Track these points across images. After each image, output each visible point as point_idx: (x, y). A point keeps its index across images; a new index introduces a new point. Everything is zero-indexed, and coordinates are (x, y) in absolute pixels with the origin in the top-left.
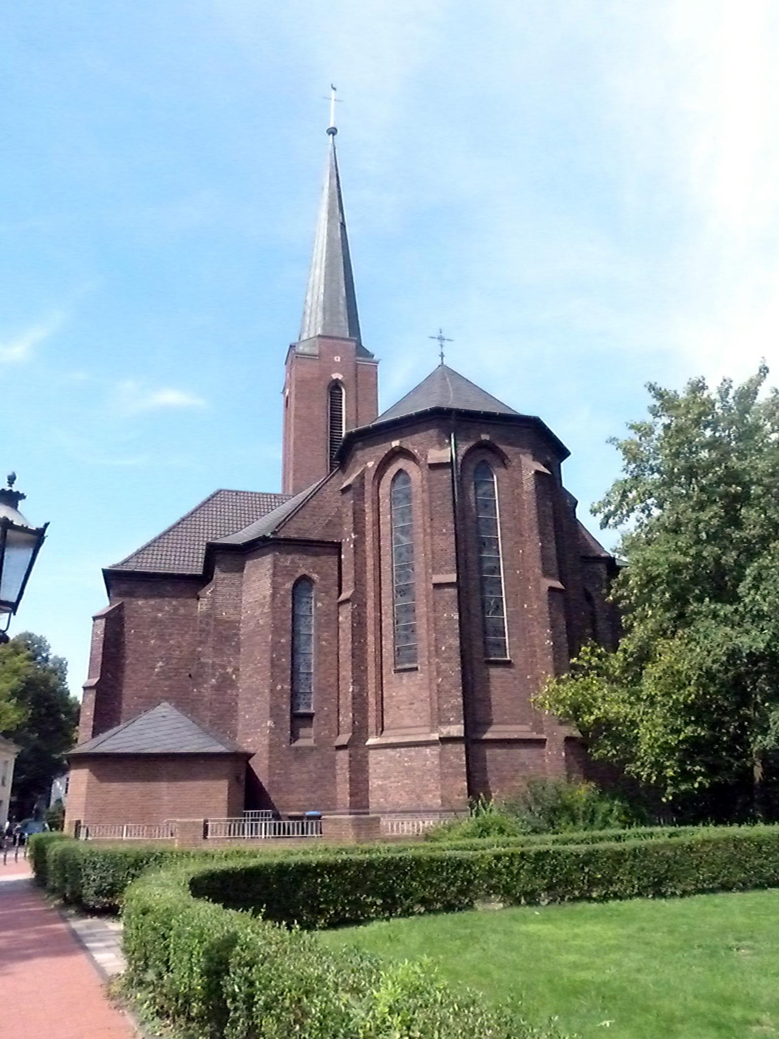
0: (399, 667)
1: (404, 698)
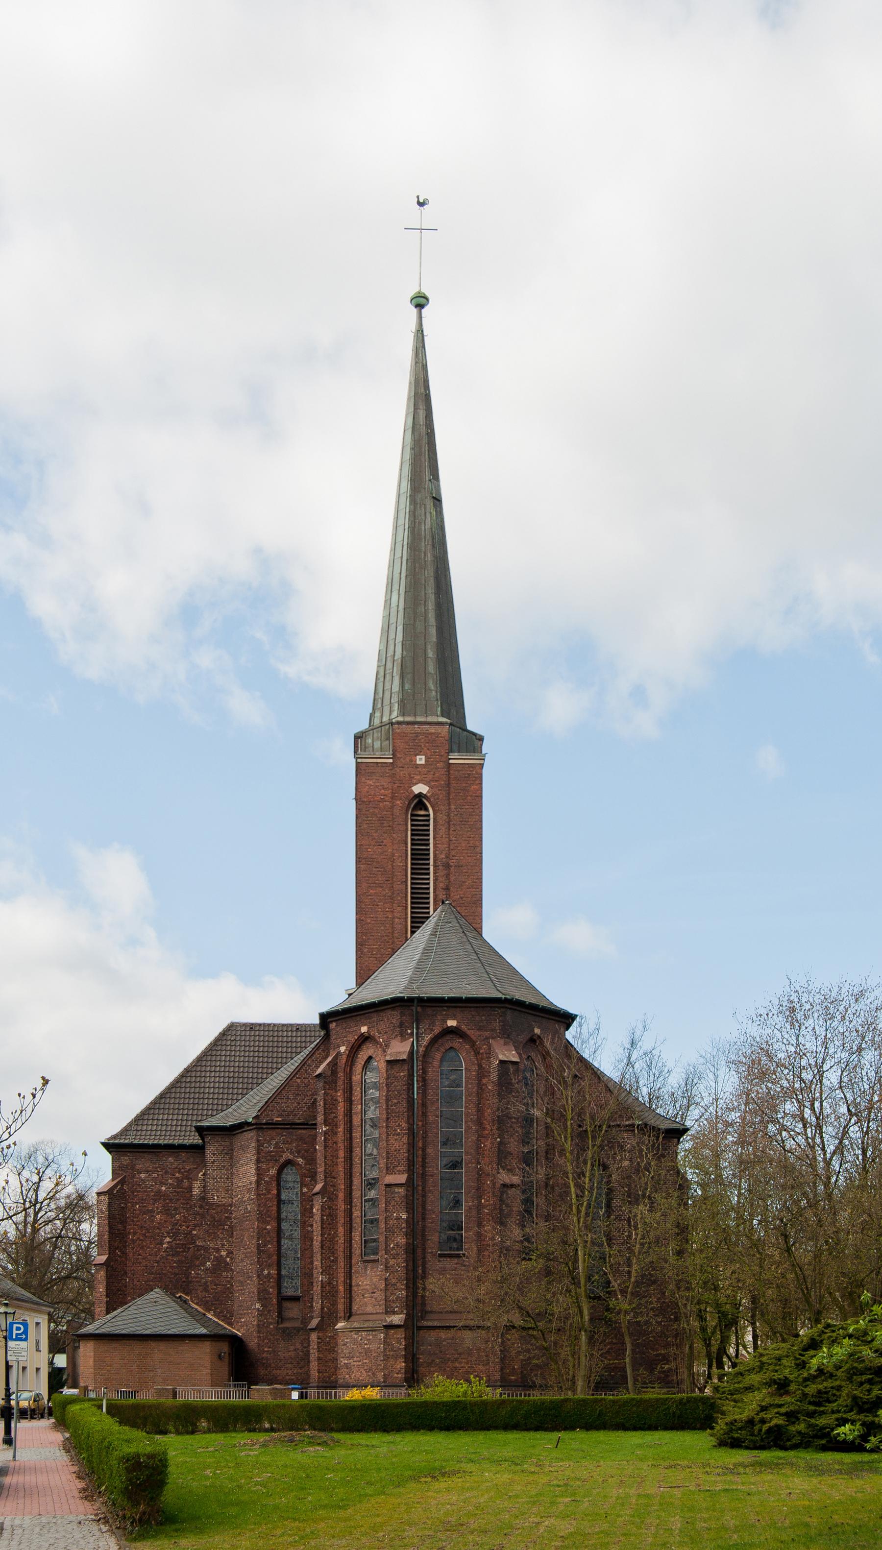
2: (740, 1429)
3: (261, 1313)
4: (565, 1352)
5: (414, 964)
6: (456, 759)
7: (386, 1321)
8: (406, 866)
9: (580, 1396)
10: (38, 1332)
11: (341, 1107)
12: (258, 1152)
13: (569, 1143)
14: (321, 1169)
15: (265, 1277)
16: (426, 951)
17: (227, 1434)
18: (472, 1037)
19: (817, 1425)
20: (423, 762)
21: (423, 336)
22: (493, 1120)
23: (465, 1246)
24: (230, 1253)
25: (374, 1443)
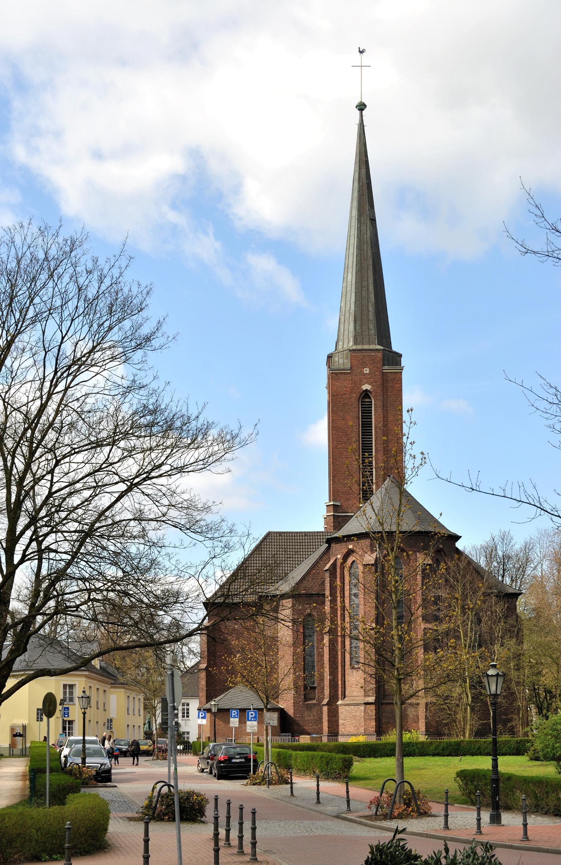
6: (387, 369)
9: (467, 739)
20: (368, 372)
21: (363, 126)
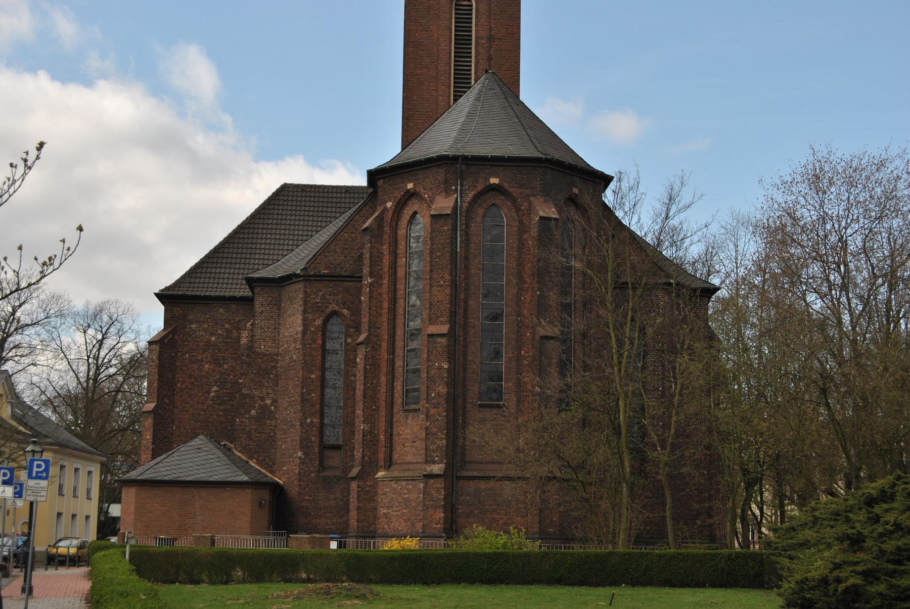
0: (407, 408)
1: (408, 436)
2: (812, 588)
3: (302, 462)
4: (605, 504)
5: (458, 126)
7: (426, 470)
8: (450, 50)
9: (621, 549)
10: (90, 481)
11: (386, 260)
12: (305, 303)
13: (610, 294)
14: (365, 320)
15: (308, 426)
16: (470, 115)
17: (261, 585)
18: (514, 194)
19: (900, 586)
22: (533, 274)
23: (505, 397)
24: (275, 401)
25: (415, 596)
